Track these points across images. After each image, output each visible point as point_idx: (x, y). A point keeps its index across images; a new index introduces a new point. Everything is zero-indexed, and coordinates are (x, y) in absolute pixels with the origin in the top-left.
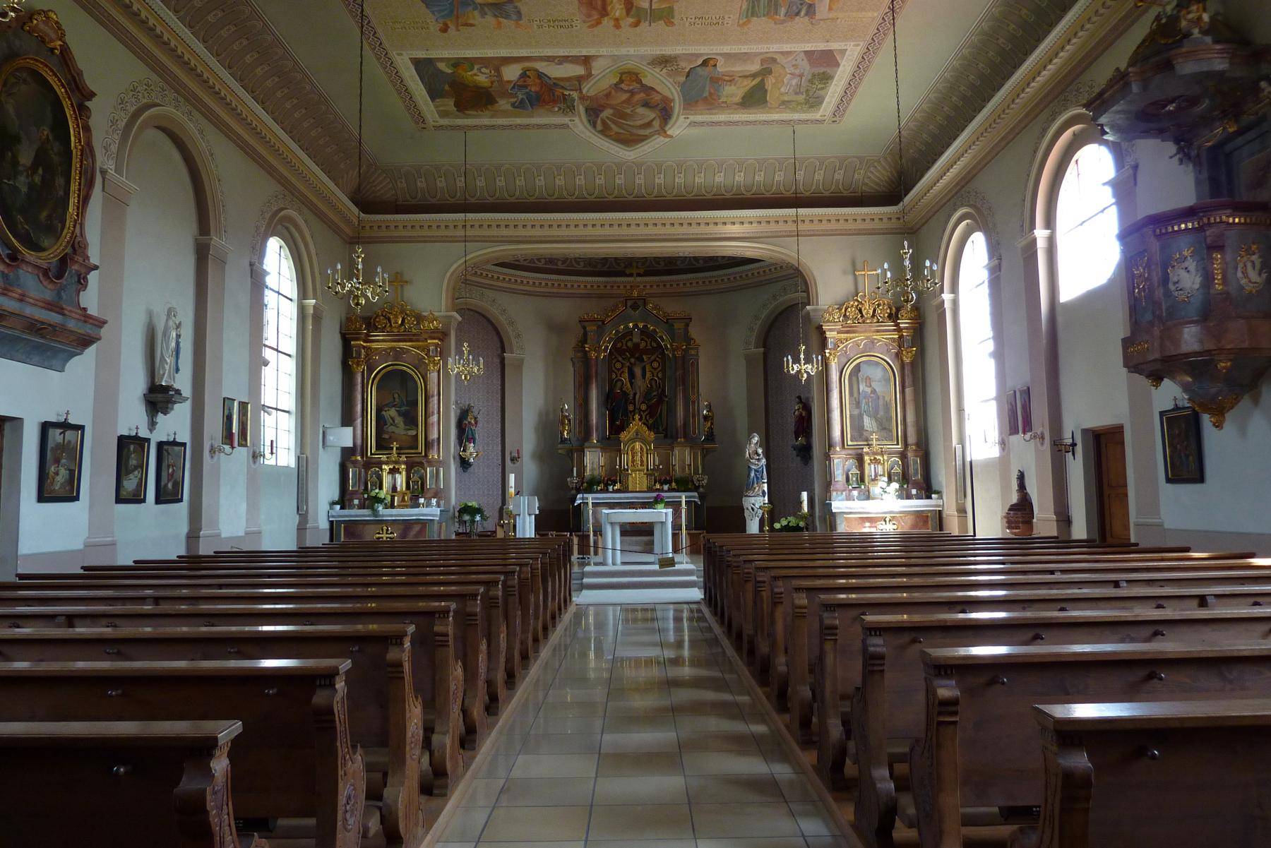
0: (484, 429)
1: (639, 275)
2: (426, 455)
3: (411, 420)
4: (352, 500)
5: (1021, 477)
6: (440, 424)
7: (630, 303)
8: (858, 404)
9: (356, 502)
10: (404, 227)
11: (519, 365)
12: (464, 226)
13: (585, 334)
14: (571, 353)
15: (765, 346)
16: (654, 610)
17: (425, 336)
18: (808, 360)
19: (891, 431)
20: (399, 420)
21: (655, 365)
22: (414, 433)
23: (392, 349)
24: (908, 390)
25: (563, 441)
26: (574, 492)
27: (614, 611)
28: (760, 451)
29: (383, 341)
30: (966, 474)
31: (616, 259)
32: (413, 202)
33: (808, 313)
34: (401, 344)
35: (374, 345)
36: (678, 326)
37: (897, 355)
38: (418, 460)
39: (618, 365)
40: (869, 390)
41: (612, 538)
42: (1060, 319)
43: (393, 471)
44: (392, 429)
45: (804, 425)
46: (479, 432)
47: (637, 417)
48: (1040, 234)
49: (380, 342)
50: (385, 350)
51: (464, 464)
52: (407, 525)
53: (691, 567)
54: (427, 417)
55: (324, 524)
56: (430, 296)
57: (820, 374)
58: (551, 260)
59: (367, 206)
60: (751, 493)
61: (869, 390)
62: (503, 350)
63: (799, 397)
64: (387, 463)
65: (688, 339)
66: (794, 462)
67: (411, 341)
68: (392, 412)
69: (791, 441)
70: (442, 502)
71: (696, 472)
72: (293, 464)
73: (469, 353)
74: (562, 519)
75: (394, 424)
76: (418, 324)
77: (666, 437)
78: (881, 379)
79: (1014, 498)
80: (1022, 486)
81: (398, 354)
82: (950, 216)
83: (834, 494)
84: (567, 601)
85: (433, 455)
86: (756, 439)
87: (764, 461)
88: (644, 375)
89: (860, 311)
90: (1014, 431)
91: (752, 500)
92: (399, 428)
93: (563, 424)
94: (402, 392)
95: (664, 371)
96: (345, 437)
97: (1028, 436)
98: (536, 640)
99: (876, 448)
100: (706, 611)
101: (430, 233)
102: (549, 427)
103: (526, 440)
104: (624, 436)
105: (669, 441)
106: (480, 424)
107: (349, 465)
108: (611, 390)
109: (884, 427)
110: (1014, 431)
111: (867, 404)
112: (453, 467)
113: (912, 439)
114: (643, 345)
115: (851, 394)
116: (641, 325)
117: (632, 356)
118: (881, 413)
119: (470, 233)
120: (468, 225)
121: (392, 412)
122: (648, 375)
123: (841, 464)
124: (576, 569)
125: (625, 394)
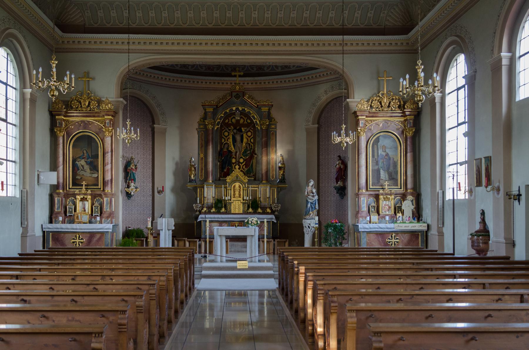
0: (141, 174)
1: (240, 76)
2: (104, 190)
3: (94, 168)
4: (57, 217)
5: (483, 213)
6: (113, 170)
7: (234, 94)
8: (377, 163)
9: (61, 219)
10: (95, 42)
11: (164, 133)
12: (128, 43)
13: (206, 113)
14: (196, 126)
15: (318, 123)
16: (245, 295)
17: (103, 113)
18: (347, 135)
19: (397, 180)
20: (87, 167)
21: (249, 134)
22: (96, 175)
23: (82, 122)
24: (409, 155)
25: (191, 181)
26: (198, 213)
27: (221, 295)
28: (314, 191)
30: (447, 209)
31: (225, 65)
32: (96, 26)
33: (348, 103)
34: (89, 119)
35: (71, 119)
36: (265, 109)
37: (403, 132)
38: (99, 193)
39: (226, 134)
40: (384, 154)
41: (220, 245)
42: (515, 113)
43: (83, 200)
44: (82, 173)
45: (342, 174)
46: (138, 175)
47: (237, 167)
48: (505, 54)
49: (75, 117)
50: (78, 122)
51: (128, 195)
52: (92, 234)
53: (270, 264)
54: (104, 165)
55: (39, 233)
56: (107, 88)
57: (354, 144)
58: (184, 66)
59: (65, 28)
60: (308, 217)
61: (384, 154)
62: (154, 123)
63: (339, 156)
64: (79, 195)
65: (269, 117)
66: (334, 196)
67: (94, 116)
68: (83, 162)
69: (332, 184)
70: (114, 220)
71: (273, 203)
72: (18, 196)
73: (131, 125)
74: (189, 230)
76: (99, 106)
77: (255, 180)
78: (393, 149)
79: (478, 227)
80: (483, 221)
81: (86, 125)
82: (442, 42)
83: (361, 219)
84: (191, 288)
85: (108, 190)
86: (312, 183)
87: (316, 197)
88: (242, 141)
89: (381, 103)
90: (479, 183)
91: (308, 221)
92: (86, 173)
93: (191, 170)
94: (88, 147)
95: (254, 138)
96: (52, 178)
97: (489, 188)
98: (170, 322)
99: (387, 191)
100: (277, 293)
101: (101, 46)
102: (182, 172)
103: (167, 179)
104: (228, 179)
105: (256, 182)
106: (138, 170)
108: (221, 149)
109: (393, 178)
110: (479, 183)
111: (383, 162)
112: (121, 198)
113: (409, 186)
114: (242, 121)
115: (373, 156)
116: (240, 109)
117: (235, 128)
118: (391, 169)
119: (132, 47)
120: (131, 42)
121: (83, 162)
122: (245, 140)
123: (365, 201)
124: (197, 265)
125: (230, 152)
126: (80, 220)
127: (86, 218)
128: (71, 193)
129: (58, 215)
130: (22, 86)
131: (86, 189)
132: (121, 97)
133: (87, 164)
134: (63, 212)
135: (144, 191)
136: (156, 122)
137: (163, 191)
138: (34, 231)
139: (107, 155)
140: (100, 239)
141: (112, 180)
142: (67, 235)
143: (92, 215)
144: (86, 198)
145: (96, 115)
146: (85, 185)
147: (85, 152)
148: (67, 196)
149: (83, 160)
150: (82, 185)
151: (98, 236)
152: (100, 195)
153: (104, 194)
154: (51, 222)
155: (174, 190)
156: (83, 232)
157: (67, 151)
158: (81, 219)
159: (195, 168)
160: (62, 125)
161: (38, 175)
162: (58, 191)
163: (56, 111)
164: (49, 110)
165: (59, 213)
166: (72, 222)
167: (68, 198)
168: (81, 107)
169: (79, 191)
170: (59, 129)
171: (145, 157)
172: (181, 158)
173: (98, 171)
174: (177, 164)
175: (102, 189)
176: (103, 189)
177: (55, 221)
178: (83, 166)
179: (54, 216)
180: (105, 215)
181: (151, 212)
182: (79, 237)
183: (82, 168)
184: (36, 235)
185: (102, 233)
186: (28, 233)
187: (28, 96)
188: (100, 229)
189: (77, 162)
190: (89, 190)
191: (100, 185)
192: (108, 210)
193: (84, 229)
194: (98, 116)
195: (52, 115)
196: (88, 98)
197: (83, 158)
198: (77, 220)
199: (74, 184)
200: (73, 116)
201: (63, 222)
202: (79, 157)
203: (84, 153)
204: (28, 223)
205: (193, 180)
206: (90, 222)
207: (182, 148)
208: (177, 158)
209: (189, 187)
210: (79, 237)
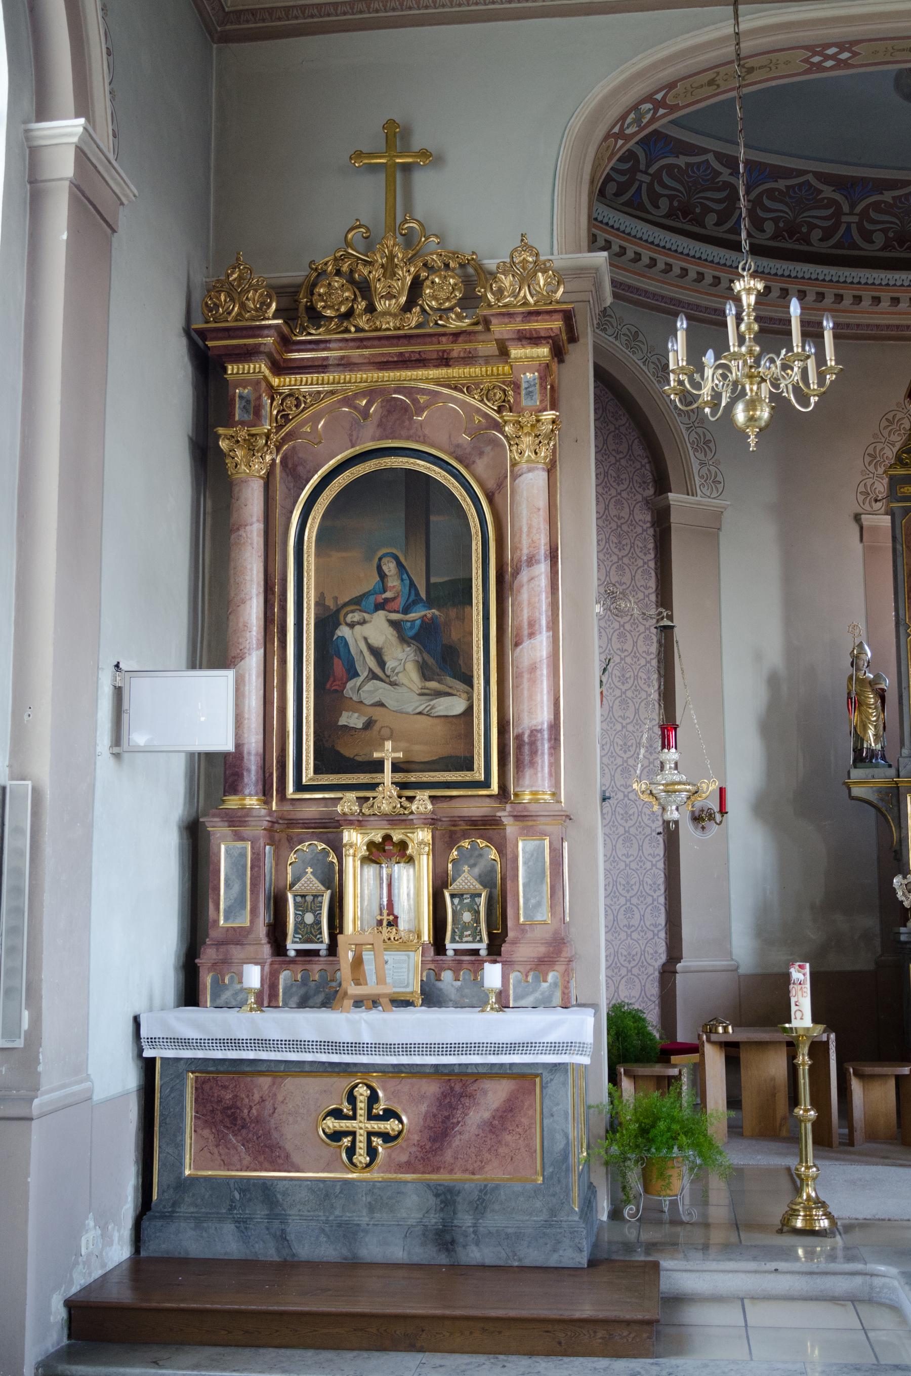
3: (445, 660)
9: (253, 976)
11: (710, 530)
20: (402, 659)
25: (862, 758)
29: (346, 365)
38: (476, 808)
43: (382, 852)
52: (455, 1085)
55: (114, 1077)
62: (662, 485)
64: (359, 823)
67: (444, 361)
68: (377, 629)
75: (381, 673)
85: (536, 786)
92: (400, 699)
93: (855, 702)
94: (418, 539)
96: (210, 711)
107: (218, 830)
121: (377, 629)
126: (371, 988)
127: (404, 970)
128: (310, 812)
129: (236, 952)
130: (28, 104)
131: (403, 786)
132: (594, 244)
133: (403, 639)
134: (261, 931)
135: (627, 817)
136: (674, 478)
137: (723, 811)
138: (79, 1069)
139: (524, 576)
140: (506, 1115)
141: (554, 727)
142: (290, 1084)
143: (439, 945)
144: (403, 845)
145: (457, 349)
146: (396, 768)
147: (390, 567)
148: (284, 831)
149: (381, 617)
150: (378, 767)
151: (495, 1095)
152: (487, 826)
153: (517, 818)
154: (190, 995)
155: (765, 808)
156: (398, 1070)
157: (288, 552)
158: (381, 980)
159: (882, 696)
160: (257, 411)
161: (118, 692)
162: (232, 802)
163: (229, 332)
164: (187, 331)
165: (237, 937)
166: (326, 996)
167: (292, 842)
168: (371, 309)
169: (363, 800)
170: (243, 434)
171: (629, 646)
172: (791, 651)
173: (468, 680)
174: (773, 681)
175: (495, 787)
176: (503, 787)
177: (219, 987)
178: (376, 653)
179: (208, 956)
180: (522, 950)
181: (662, 920)
182: (373, 1099)
183: (371, 662)
184: (98, 1096)
185: (525, 1078)
186: (35, 1089)
187: (64, 167)
188: (513, 1048)
189: (343, 631)
190: (422, 796)
191: (485, 759)
192: (543, 914)
193: (407, 1048)
194: (469, 359)
195: (208, 363)
196: (410, 261)
197: (379, 607)
198: (353, 990)
199: (329, 759)
200: (321, 367)
201: (268, 997)
202: (357, 602)
203: (382, 575)
204: (36, 1021)
205: (872, 754)
206: (431, 997)
207: (793, 607)
208: (774, 656)
209: (857, 791)
210: (373, 1099)
